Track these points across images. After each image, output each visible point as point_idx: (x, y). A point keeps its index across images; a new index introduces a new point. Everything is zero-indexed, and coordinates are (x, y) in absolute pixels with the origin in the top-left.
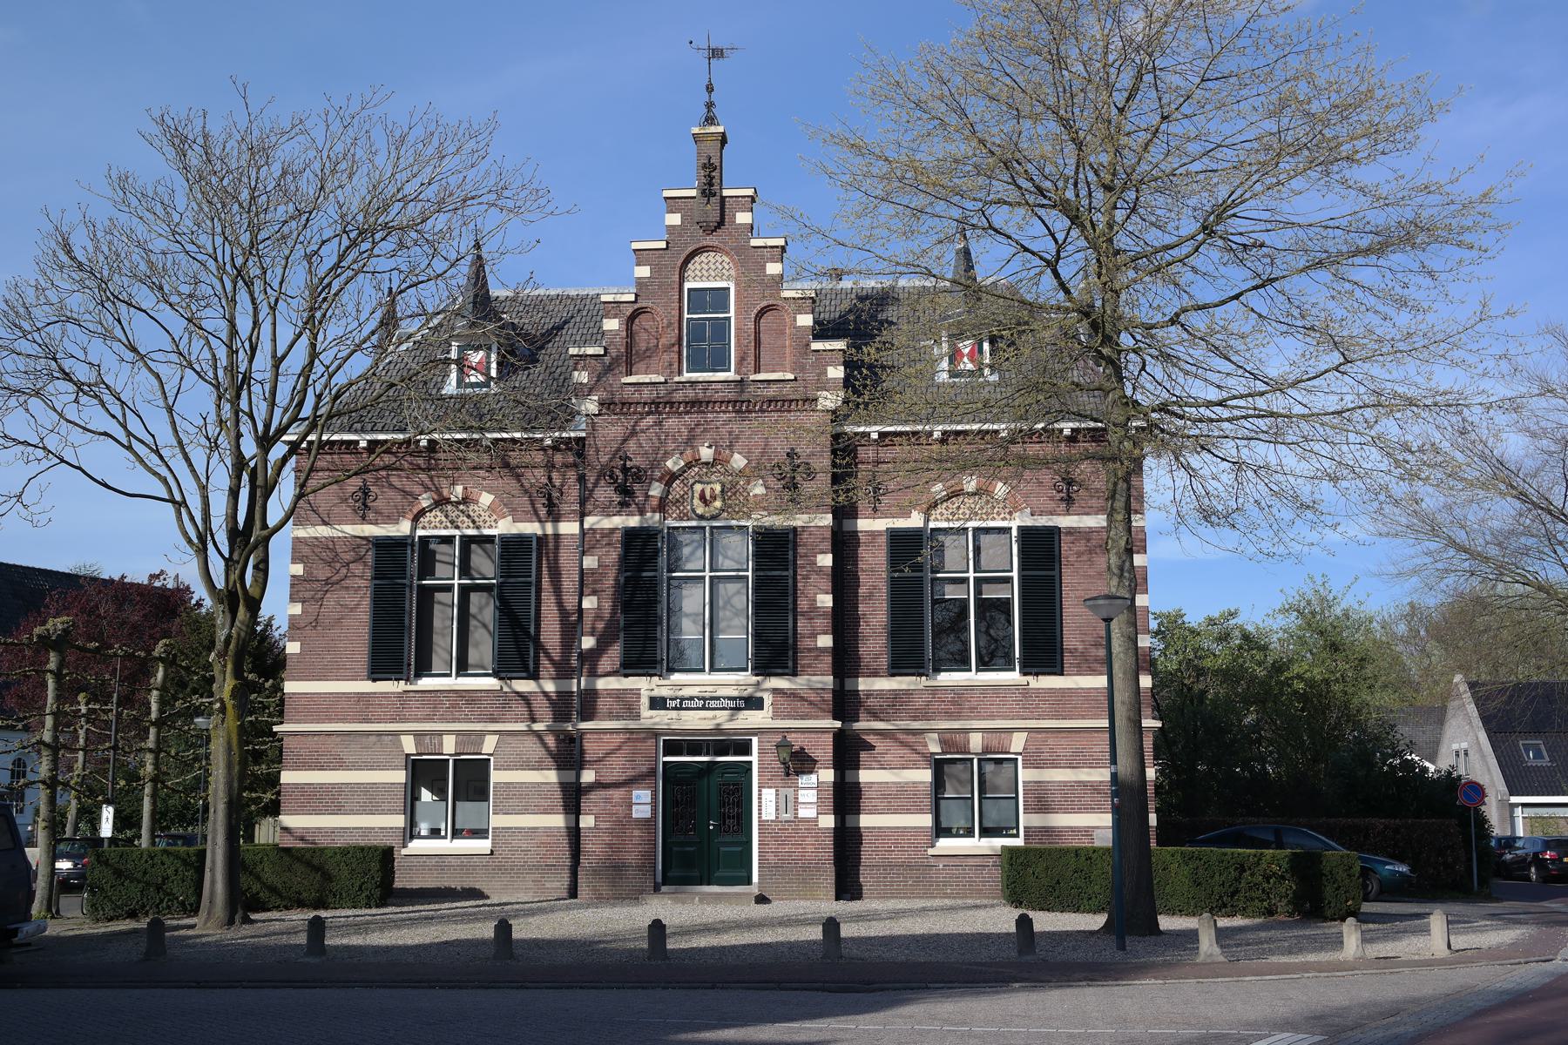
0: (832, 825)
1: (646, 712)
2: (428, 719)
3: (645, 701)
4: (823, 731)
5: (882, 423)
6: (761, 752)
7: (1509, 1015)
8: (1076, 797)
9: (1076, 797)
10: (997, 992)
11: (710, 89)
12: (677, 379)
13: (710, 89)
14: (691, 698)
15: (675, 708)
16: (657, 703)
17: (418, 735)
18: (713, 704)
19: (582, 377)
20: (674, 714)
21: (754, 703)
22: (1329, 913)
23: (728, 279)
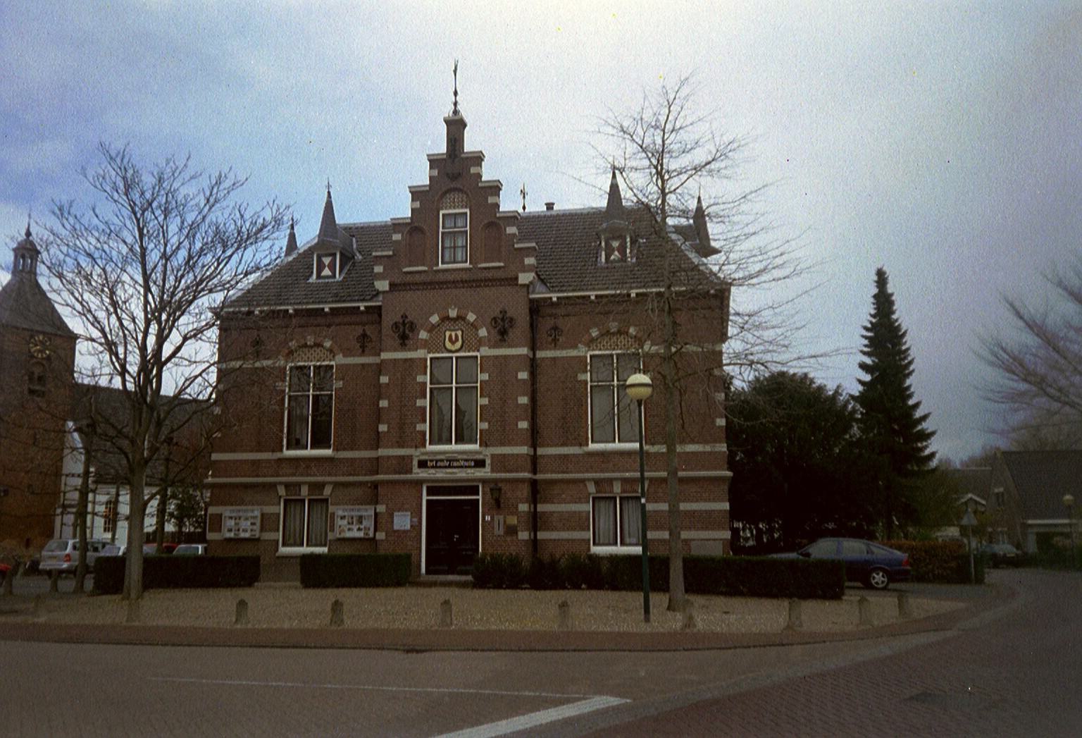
0: (728, 508)
1: (415, 469)
2: (293, 475)
3: (415, 463)
4: (522, 481)
5: (559, 291)
6: (484, 493)
7: (456, 455)
8: (705, 521)
9: (705, 521)
10: (628, 553)
11: (456, 93)
12: (435, 268)
13: (456, 93)
14: (442, 460)
15: (433, 467)
16: (423, 464)
17: (287, 486)
18: (455, 464)
19: (378, 269)
20: (433, 471)
21: (480, 464)
22: (555, 501)
23: (466, 207)
